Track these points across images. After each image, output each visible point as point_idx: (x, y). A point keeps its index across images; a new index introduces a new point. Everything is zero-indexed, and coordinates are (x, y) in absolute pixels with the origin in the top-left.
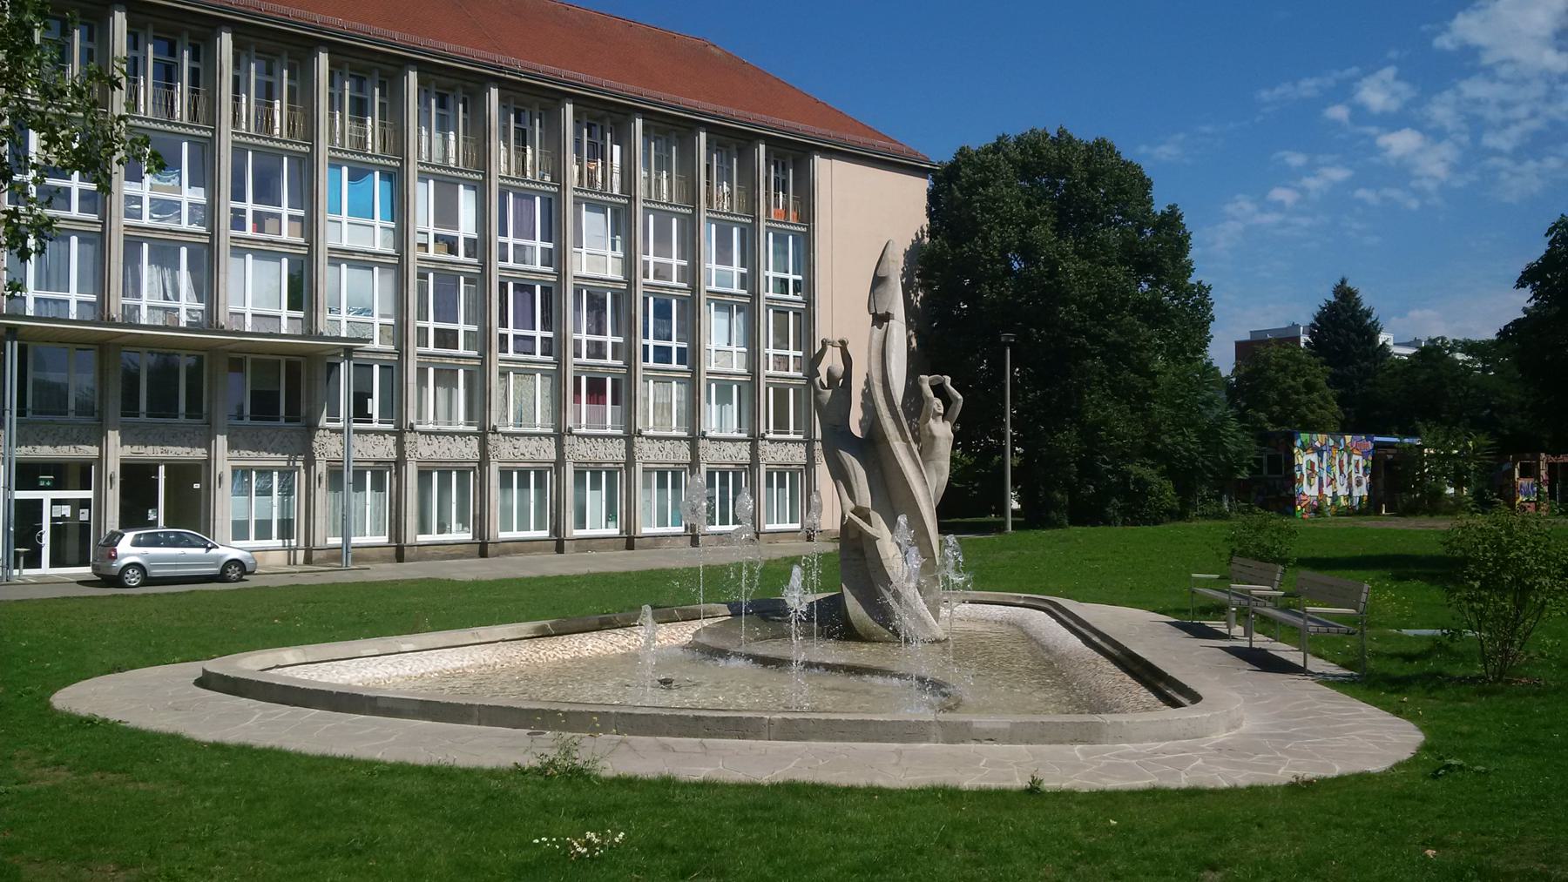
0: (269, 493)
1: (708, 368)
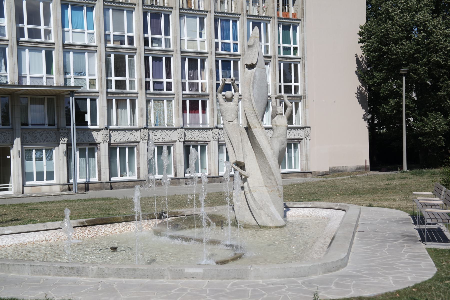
0: (41, 159)
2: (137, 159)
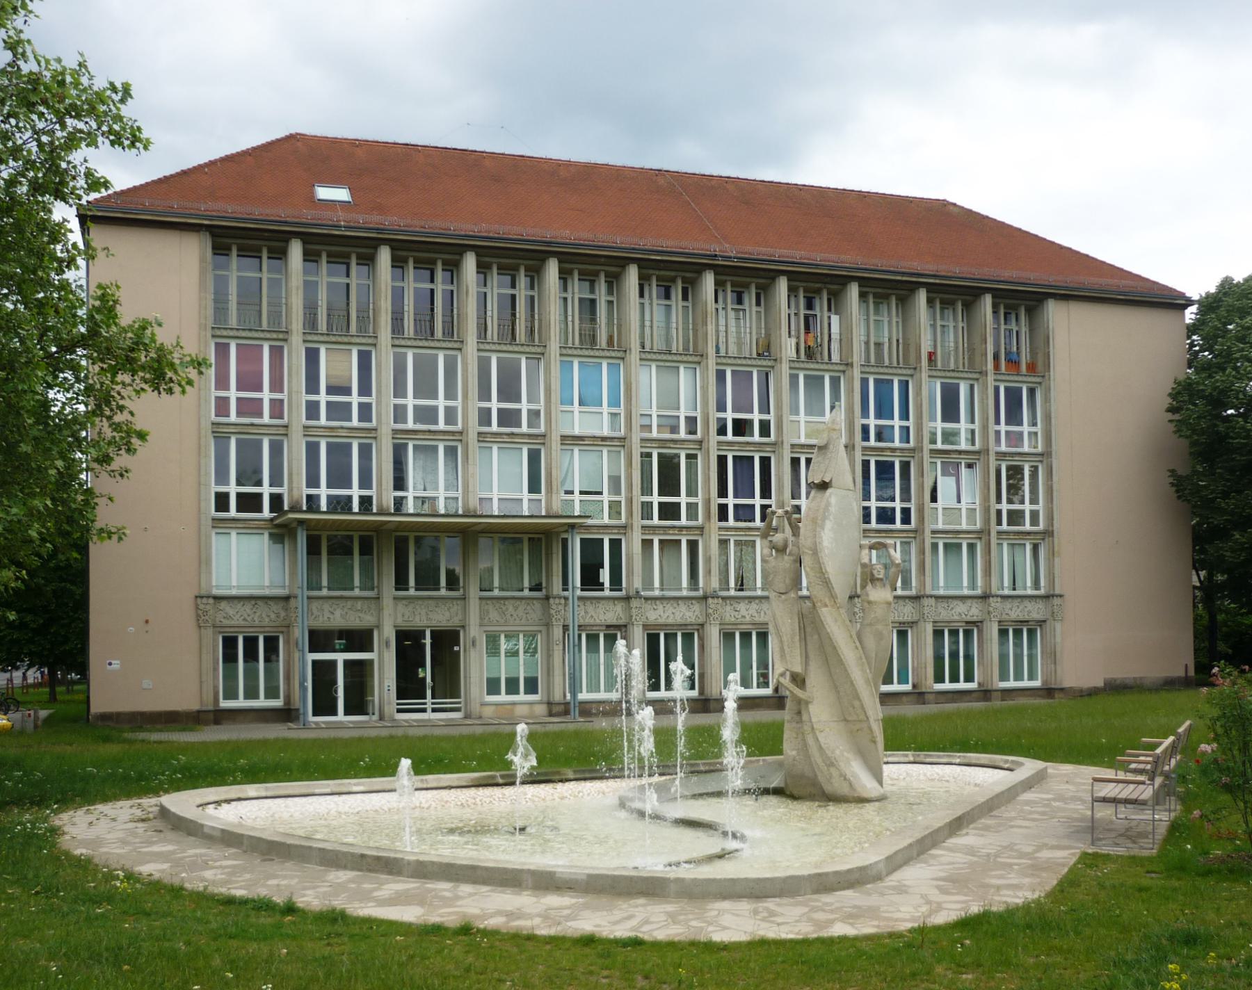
0: (516, 654)
1: (934, 527)
2: (979, 647)
